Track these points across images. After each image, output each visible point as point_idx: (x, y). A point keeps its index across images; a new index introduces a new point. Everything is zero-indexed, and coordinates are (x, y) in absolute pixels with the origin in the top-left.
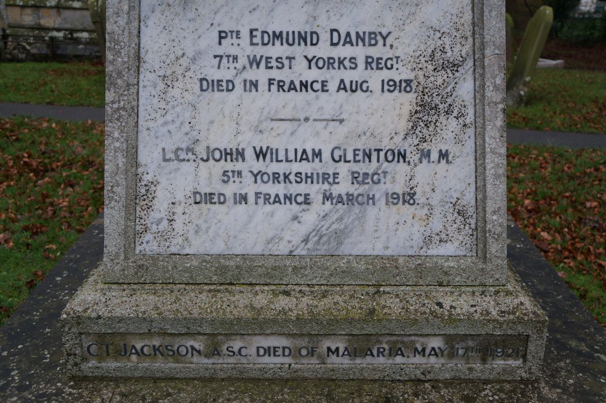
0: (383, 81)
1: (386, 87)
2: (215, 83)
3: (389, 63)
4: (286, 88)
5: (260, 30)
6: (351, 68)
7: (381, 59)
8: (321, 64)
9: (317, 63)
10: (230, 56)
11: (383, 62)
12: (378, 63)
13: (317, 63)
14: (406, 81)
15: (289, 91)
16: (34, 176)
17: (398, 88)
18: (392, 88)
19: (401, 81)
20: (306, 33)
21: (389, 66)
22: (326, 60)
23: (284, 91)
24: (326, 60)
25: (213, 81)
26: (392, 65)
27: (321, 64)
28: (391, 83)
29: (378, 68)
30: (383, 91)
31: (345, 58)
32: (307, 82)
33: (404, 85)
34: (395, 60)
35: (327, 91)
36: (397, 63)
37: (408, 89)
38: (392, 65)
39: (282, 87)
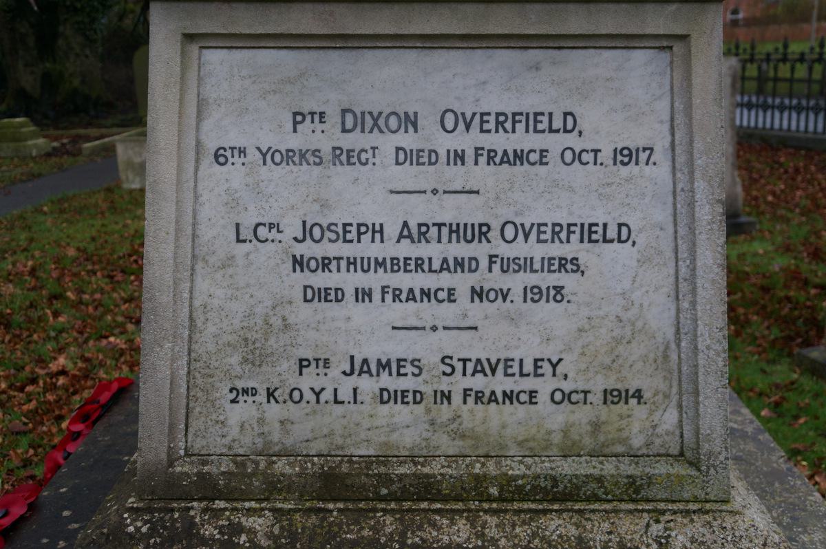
0: (525, 289)
1: (529, 295)
2: (415, 153)
3: (364, 156)
4: (403, 297)
5: (413, 259)
6: (315, 164)
7: (353, 151)
8: (278, 158)
9: (487, 296)
10: (342, 258)
11: (355, 154)
12: (349, 157)
13: (487, 296)
14: (555, 288)
15: (407, 301)
16: (15, 287)
17: (544, 298)
18: (537, 297)
19: (548, 288)
20: (463, 259)
21: (364, 161)
22: (284, 153)
23: (401, 301)
24: (284, 153)
25: (319, 289)
26: (367, 159)
27: (278, 158)
28: (536, 290)
29: (349, 163)
30: (525, 301)
31: (308, 151)
32: (429, 289)
33: (552, 292)
34: (370, 152)
35: (455, 301)
36: (374, 157)
37: (559, 297)
38: (367, 159)
39: (398, 296)
